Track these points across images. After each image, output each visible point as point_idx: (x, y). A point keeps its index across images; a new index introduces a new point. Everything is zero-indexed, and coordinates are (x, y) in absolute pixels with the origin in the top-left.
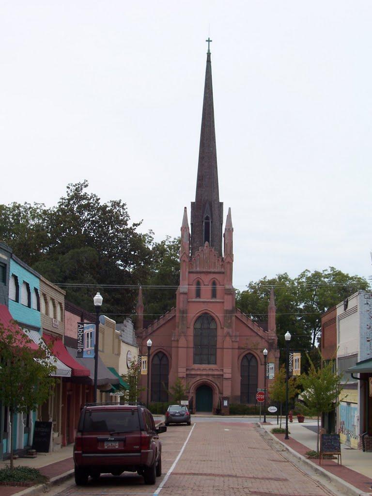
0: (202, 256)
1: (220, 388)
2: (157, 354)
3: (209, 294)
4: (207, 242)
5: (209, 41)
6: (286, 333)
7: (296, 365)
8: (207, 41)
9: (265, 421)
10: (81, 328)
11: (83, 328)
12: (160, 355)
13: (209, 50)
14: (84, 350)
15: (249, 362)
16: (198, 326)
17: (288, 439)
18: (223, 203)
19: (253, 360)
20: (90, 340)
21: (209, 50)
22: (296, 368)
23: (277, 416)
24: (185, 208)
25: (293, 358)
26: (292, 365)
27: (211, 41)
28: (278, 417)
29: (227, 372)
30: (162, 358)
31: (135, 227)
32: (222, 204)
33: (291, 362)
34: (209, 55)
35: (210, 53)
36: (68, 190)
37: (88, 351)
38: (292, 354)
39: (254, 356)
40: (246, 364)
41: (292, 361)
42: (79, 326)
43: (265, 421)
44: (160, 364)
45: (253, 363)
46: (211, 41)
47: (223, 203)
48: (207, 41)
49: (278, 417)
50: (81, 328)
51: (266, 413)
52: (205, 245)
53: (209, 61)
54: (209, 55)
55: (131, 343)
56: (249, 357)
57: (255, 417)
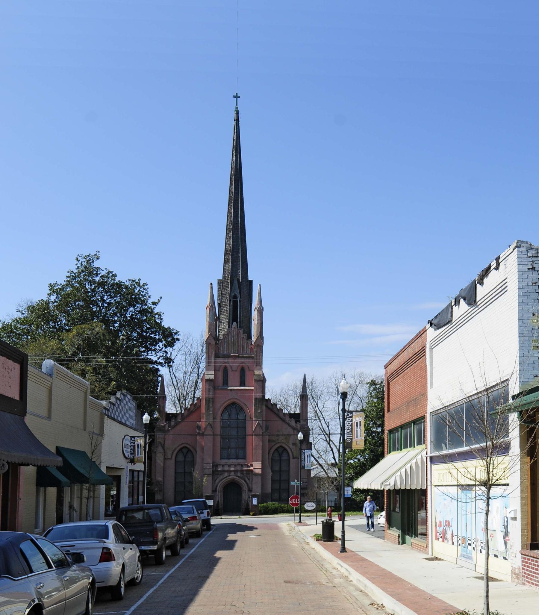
0: (230, 339)
1: (250, 485)
2: (180, 450)
3: (237, 380)
4: (235, 323)
5: (237, 97)
6: (299, 433)
7: (307, 460)
8: (234, 97)
9: (300, 521)
10: (133, 441)
11: (134, 440)
12: (185, 451)
13: (237, 108)
14: (135, 457)
15: (280, 455)
16: (226, 416)
17: (346, 552)
18: (252, 281)
19: (285, 454)
20: (139, 450)
21: (237, 108)
22: (307, 463)
23: (315, 514)
24: (211, 284)
25: (305, 454)
26: (305, 460)
27: (239, 97)
28: (317, 515)
29: (257, 467)
30: (186, 454)
31: (155, 306)
32: (251, 282)
33: (303, 457)
34: (237, 113)
35: (238, 111)
36: (77, 262)
37: (137, 458)
38: (304, 451)
39: (285, 449)
40: (277, 457)
41: (304, 457)
42: (131, 439)
43: (300, 521)
44: (185, 461)
45: (284, 457)
46: (239, 97)
47: (252, 281)
48: (234, 97)
49: (317, 515)
50: (133, 441)
51: (300, 510)
52: (233, 326)
53: (237, 120)
54: (237, 113)
55: (133, 426)
56: (280, 450)
57: (288, 517)
